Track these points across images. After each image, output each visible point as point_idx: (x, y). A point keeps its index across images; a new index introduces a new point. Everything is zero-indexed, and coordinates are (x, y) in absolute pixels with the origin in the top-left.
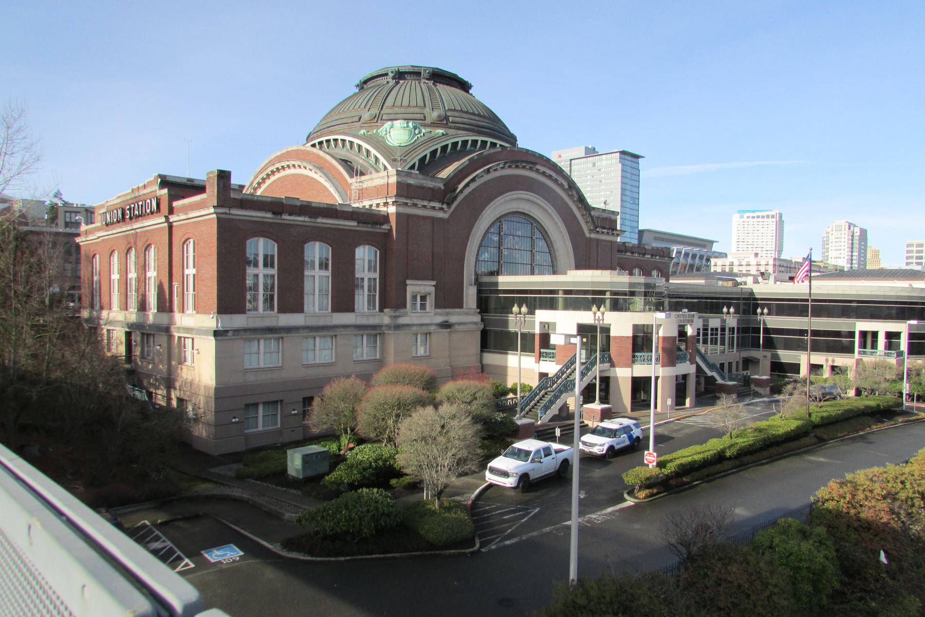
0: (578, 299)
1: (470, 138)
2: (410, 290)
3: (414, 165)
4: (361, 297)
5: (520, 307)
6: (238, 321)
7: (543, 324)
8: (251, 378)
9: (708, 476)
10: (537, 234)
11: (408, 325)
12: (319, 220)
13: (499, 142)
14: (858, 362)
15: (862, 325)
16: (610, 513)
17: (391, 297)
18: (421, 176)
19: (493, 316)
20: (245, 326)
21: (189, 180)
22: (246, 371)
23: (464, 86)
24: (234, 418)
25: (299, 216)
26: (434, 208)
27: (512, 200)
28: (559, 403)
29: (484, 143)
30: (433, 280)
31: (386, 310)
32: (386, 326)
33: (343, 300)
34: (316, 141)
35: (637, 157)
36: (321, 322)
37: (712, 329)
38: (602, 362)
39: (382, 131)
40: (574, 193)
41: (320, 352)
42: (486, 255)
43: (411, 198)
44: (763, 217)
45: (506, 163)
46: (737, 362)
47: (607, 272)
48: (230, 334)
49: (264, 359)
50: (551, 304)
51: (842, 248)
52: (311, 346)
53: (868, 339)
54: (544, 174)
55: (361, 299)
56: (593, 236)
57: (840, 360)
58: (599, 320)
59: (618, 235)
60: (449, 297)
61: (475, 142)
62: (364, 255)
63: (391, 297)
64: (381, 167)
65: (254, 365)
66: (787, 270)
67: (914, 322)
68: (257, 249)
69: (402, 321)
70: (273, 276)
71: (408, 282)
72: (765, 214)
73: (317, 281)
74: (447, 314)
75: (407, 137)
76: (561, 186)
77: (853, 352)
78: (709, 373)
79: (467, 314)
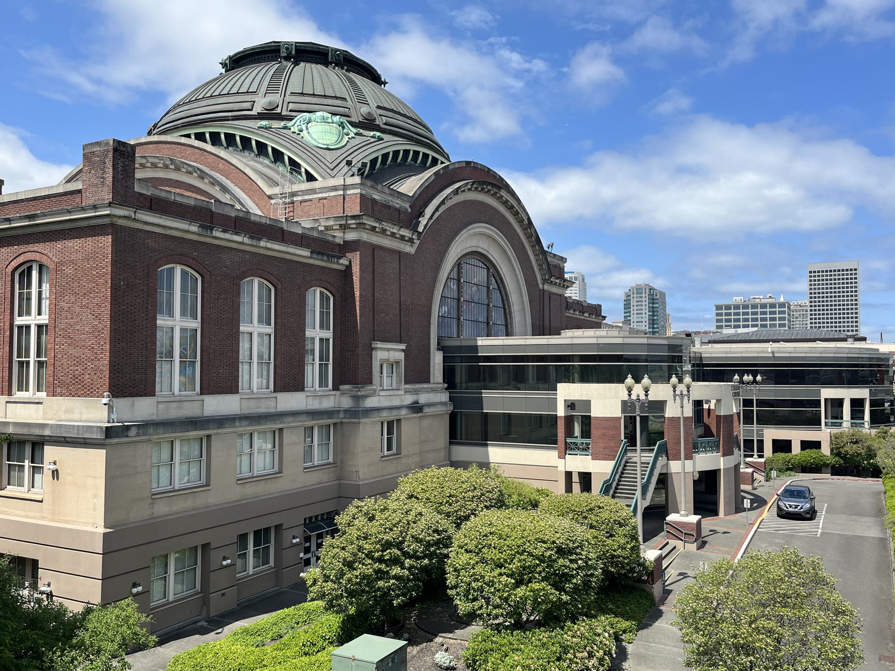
1: (413, 148)
6: (142, 409)
7: (571, 405)
8: (162, 508)
10: (493, 285)
11: (378, 410)
12: (262, 243)
15: (828, 393)
19: (465, 393)
20: (154, 417)
25: (236, 234)
26: (402, 238)
31: (342, 387)
32: (346, 411)
34: (207, 130)
39: (295, 125)
43: (380, 220)
48: (133, 432)
50: (587, 375)
51: (643, 312)
55: (312, 373)
56: (546, 287)
57: (810, 435)
63: (350, 369)
69: (371, 403)
71: (379, 345)
75: (335, 138)
79: (434, 391)
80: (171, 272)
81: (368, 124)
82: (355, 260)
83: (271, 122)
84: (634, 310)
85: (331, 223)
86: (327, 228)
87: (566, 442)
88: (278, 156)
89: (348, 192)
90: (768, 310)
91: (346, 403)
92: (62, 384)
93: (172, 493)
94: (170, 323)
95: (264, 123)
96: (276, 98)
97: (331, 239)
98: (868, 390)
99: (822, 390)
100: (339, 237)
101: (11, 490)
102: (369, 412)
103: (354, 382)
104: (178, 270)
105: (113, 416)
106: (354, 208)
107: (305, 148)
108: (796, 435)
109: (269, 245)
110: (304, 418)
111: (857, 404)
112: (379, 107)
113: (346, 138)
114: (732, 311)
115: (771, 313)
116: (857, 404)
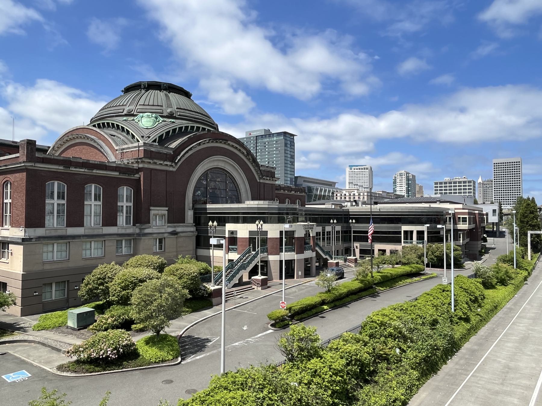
0: (247, 217)
2: (152, 213)
3: (156, 139)
4: (121, 217)
5: (213, 222)
7: (232, 232)
8: (47, 267)
9: (316, 313)
12: (94, 171)
13: (207, 128)
14: (403, 247)
15: (405, 228)
16: (259, 337)
17: (140, 217)
18: (159, 147)
20: (44, 235)
21: (13, 142)
22: (44, 263)
23: (187, 95)
24: (35, 292)
26: (167, 165)
27: (214, 160)
28: (238, 276)
29: (198, 128)
30: (166, 207)
32: (137, 234)
33: (110, 218)
34: (96, 123)
35: (293, 135)
36: (96, 232)
37: (327, 232)
38: (262, 252)
40: (250, 157)
41: (94, 250)
42: (199, 192)
43: (152, 159)
44: (362, 169)
45: (210, 140)
46: (342, 250)
47: (266, 202)
48: (34, 240)
49: (57, 255)
50: (236, 220)
52: (88, 246)
53: (408, 235)
54: (233, 146)
55: (121, 219)
56: (261, 181)
58: (260, 229)
59: (276, 181)
60: (176, 217)
61: (192, 127)
62: (125, 191)
63: (140, 217)
64: (136, 140)
65: (50, 259)
66: (374, 199)
67: (428, 225)
68: (53, 189)
69: (147, 231)
70: (64, 204)
71: (152, 208)
72: (363, 167)
73: (93, 207)
74: (175, 227)
76: (243, 153)
77: (401, 242)
78: (324, 257)
80: (53, 184)
81: (171, 116)
82: (142, 174)
83: (128, 117)
84: (398, 184)
85: (133, 161)
86: (132, 163)
87: (229, 248)
88: (128, 132)
89: (140, 148)
90: (462, 184)
91: (137, 231)
92: (15, 224)
93: (54, 262)
94: (52, 202)
95: (125, 118)
96: (132, 107)
97: (131, 167)
98: (321, 227)
99: (402, 227)
100: (135, 166)
101: (3, 260)
102: (146, 235)
103: (140, 223)
104: (56, 183)
105: (27, 234)
106: (142, 155)
107: (138, 129)
108: (388, 247)
109: (97, 172)
110: (115, 236)
111: (420, 234)
112: (177, 108)
113: (157, 123)
114: (448, 185)
115: (445, 187)
116: (420, 234)
